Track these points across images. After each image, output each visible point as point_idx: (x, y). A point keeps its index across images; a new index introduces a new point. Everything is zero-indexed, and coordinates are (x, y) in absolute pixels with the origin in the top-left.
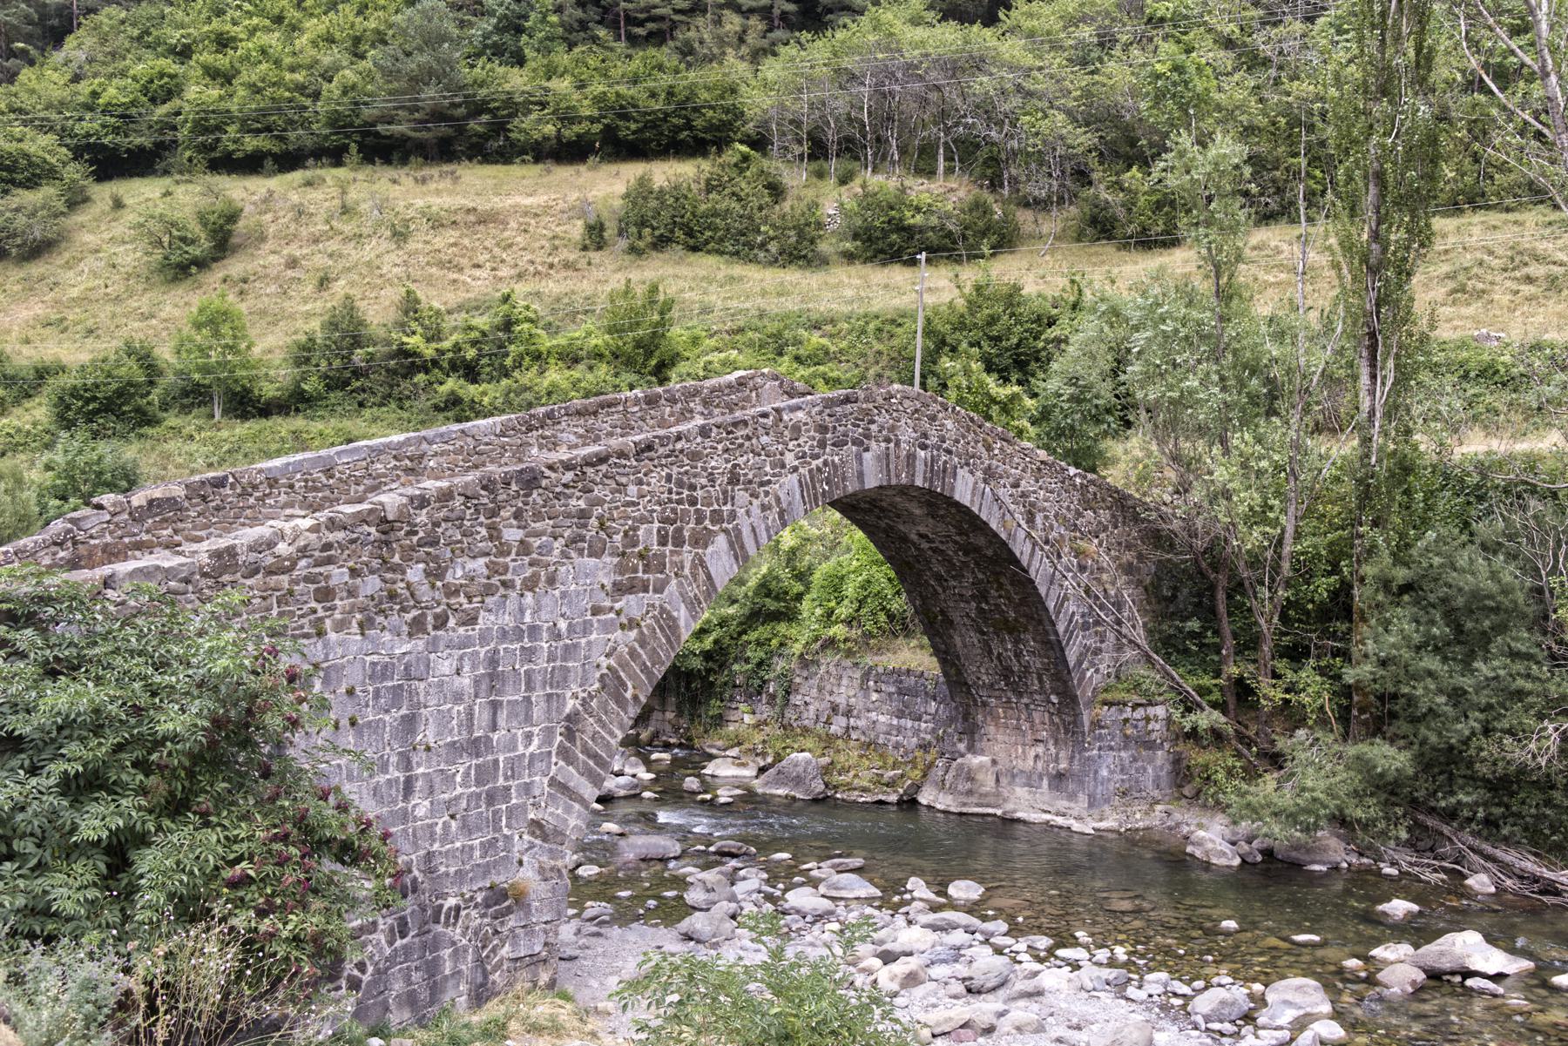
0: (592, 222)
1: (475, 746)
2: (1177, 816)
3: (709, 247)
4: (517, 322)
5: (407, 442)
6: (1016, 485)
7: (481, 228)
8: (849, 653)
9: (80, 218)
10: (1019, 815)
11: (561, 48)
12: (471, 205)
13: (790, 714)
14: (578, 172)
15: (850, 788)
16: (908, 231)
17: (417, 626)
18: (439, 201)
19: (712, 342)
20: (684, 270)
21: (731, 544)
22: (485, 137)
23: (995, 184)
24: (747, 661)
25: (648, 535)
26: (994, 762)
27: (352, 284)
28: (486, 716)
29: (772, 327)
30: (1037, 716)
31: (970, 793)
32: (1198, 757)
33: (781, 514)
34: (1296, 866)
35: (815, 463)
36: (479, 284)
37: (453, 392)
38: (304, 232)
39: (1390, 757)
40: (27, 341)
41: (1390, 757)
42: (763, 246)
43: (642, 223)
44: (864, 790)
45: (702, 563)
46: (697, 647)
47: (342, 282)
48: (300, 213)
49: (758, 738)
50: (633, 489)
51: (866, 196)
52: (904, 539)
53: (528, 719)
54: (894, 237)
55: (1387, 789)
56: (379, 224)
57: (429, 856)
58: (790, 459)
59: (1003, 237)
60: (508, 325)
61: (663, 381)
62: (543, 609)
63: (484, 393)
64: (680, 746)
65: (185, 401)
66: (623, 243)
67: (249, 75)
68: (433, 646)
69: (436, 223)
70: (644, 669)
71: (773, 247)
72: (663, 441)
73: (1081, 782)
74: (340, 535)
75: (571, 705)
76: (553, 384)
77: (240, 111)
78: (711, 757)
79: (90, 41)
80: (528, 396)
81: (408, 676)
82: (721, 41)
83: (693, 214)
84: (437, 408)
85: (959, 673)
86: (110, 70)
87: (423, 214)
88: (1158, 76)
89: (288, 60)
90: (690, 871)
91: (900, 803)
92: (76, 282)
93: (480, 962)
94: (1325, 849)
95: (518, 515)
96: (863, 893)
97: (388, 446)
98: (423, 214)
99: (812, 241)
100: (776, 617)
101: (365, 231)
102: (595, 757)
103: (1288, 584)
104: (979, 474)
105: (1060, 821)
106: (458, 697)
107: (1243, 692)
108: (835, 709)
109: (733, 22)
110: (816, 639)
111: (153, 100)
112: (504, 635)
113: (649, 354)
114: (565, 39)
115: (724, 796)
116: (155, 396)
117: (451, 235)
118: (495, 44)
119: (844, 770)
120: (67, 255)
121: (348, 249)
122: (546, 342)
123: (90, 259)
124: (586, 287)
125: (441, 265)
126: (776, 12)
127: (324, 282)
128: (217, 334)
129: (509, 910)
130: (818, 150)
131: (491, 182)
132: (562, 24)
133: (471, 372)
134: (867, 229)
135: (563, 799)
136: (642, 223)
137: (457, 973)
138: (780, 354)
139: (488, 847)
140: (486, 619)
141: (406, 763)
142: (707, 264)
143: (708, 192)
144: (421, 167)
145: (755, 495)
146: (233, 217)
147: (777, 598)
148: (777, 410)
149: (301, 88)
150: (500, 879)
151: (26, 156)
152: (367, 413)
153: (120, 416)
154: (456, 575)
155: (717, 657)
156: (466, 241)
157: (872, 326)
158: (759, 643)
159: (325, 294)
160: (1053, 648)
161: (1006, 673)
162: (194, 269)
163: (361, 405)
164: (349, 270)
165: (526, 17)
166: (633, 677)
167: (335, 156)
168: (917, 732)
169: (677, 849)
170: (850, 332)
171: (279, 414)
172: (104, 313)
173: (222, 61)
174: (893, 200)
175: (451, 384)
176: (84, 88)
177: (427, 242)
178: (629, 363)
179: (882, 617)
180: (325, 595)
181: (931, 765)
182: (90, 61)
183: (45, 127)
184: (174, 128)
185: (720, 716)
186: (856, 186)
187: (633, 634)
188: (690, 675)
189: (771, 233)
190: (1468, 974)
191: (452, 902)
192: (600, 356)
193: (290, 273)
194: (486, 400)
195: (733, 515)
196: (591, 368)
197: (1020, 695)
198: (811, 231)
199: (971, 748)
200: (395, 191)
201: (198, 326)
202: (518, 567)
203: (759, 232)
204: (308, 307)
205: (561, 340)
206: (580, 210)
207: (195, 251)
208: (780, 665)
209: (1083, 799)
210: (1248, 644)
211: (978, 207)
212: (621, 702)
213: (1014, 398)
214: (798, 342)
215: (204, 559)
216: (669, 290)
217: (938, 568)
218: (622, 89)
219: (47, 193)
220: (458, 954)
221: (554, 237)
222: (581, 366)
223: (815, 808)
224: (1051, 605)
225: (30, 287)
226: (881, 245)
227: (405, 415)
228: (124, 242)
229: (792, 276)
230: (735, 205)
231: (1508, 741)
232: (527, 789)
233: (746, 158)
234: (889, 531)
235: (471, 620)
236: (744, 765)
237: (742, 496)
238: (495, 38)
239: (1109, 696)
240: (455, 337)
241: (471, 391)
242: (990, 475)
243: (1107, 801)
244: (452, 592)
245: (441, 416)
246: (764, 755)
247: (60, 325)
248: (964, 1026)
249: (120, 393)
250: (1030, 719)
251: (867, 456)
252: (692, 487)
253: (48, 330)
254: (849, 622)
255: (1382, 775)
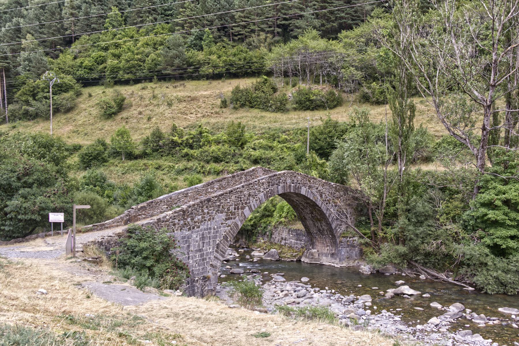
0: (223, 100)
1: (200, 250)
2: (360, 263)
3: (256, 106)
4: (203, 133)
5: (185, 191)
6: (317, 189)
7: (192, 102)
8: (285, 225)
9: (80, 99)
10: (324, 263)
11: (213, 44)
12: (189, 95)
13: (272, 240)
14: (219, 83)
15: (285, 257)
16: (311, 101)
17: (190, 229)
18: (180, 94)
19: (256, 137)
20: (249, 114)
21: (249, 209)
22: (192, 73)
23: (336, 86)
24: (262, 227)
25: (232, 208)
26: (318, 251)
27: (157, 119)
28: (202, 245)
29: (272, 133)
30: (327, 240)
31: (312, 258)
32: (365, 249)
33: (260, 201)
34: (383, 274)
35: (267, 190)
36: (192, 118)
37: (186, 152)
38: (143, 104)
39: (402, 249)
40: (69, 137)
41: (402, 249)
42: (271, 106)
43: (237, 100)
44: (288, 258)
45: (243, 213)
46: (249, 224)
47: (154, 119)
48: (142, 98)
49: (264, 246)
50: (229, 200)
51: (300, 91)
52: (293, 201)
53: (210, 245)
54: (307, 103)
55: (403, 256)
56: (164, 101)
57: (193, 270)
58: (262, 190)
59: (338, 102)
60: (201, 133)
61: (243, 148)
62: (212, 224)
63: (195, 152)
64: (246, 248)
65: (114, 155)
66: (232, 106)
67: (124, 57)
68: (192, 232)
69: (180, 101)
70: (232, 234)
71: (274, 107)
72: (234, 189)
73: (337, 255)
74: (176, 214)
75: (217, 242)
76: (213, 150)
77: (123, 67)
78: (254, 250)
79: (79, 46)
80: (207, 153)
81: (188, 238)
82: (260, 42)
83: (251, 97)
84: (182, 157)
85: (309, 230)
86: (85, 55)
87: (176, 98)
88: (381, 56)
89: (136, 51)
90: (245, 275)
91: (297, 261)
92: (81, 119)
93: (202, 290)
94: (389, 270)
95: (207, 207)
96: (282, 280)
97: (181, 192)
98: (176, 98)
99: (284, 105)
100: (268, 216)
101: (160, 103)
102: (222, 252)
103: (384, 208)
104: (307, 187)
105: (333, 264)
106: (197, 241)
107: (375, 234)
108: (282, 238)
109: (263, 36)
110: (278, 222)
111: (98, 64)
112: (205, 229)
113: (239, 141)
114: (214, 41)
115: (255, 260)
116: (106, 154)
117: (184, 104)
118: (194, 44)
119: (284, 253)
120: (77, 111)
121: (155, 109)
122: (211, 138)
123: (84, 112)
124: (221, 120)
125: (181, 113)
126: (276, 31)
127: (149, 119)
128: (123, 137)
129: (207, 281)
130: (286, 74)
131: (194, 87)
132: (214, 37)
133: (191, 147)
134: (300, 101)
135: (216, 260)
136: (237, 100)
137: (198, 292)
138: (274, 140)
139: (203, 269)
140: (201, 227)
141: (188, 254)
142: (255, 112)
143: (256, 90)
144: (174, 83)
145: (254, 198)
146: (123, 100)
147: (268, 212)
148: (259, 180)
149: (140, 60)
150: (205, 275)
151: (65, 83)
152: (164, 158)
153: (98, 160)
154: (196, 219)
155: (254, 226)
156: (188, 106)
157: (299, 132)
158: (264, 223)
159: (150, 122)
160: (329, 225)
161: (319, 230)
162: (113, 115)
163: (162, 156)
164: (156, 115)
165: (203, 35)
166: (230, 236)
167: (150, 80)
168: (301, 244)
169: (243, 271)
170: (293, 133)
171: (140, 158)
172: (89, 129)
173: (117, 52)
174: (307, 92)
175: (186, 150)
176: (78, 61)
177: (177, 107)
178: (234, 144)
179: (293, 216)
180: (174, 225)
181: (304, 252)
182: (80, 52)
183: (68, 73)
184: (104, 72)
185: (256, 240)
186: (297, 87)
187: (229, 228)
188: (248, 231)
189: (273, 103)
190: (404, 294)
191: (197, 279)
192: (225, 142)
193: (140, 116)
194: (195, 154)
195: (249, 203)
196: (223, 145)
197: (323, 235)
198: (284, 102)
199: (313, 248)
200: (168, 91)
201: (118, 135)
202: (207, 217)
203: (269, 102)
204: (145, 126)
205: (215, 137)
206: (220, 96)
207: (113, 110)
208: (269, 228)
209: (338, 260)
210: (376, 222)
211: (332, 94)
212: (227, 241)
213: (323, 163)
214: (279, 137)
215: (156, 220)
216: (244, 122)
217: (301, 207)
218: (231, 58)
219: (70, 94)
220: (198, 288)
221: (213, 104)
222: (221, 145)
223: (277, 262)
224: (327, 215)
225: (68, 121)
226: (304, 105)
227: (174, 159)
228: (93, 107)
229: (278, 115)
230: (263, 94)
231: (426, 245)
232: (210, 258)
233: (266, 80)
234: (289, 199)
235: (199, 227)
236: (261, 252)
237: (251, 198)
238: (194, 42)
239: (343, 235)
240: (186, 137)
241: (192, 152)
242: (310, 187)
243: (344, 260)
244: (195, 222)
245: (183, 159)
246: (266, 250)
247: (77, 132)
248: (294, 302)
249: (98, 154)
250: (325, 241)
251: (279, 187)
252: (241, 198)
253: (74, 134)
254: (285, 217)
255: (401, 253)
